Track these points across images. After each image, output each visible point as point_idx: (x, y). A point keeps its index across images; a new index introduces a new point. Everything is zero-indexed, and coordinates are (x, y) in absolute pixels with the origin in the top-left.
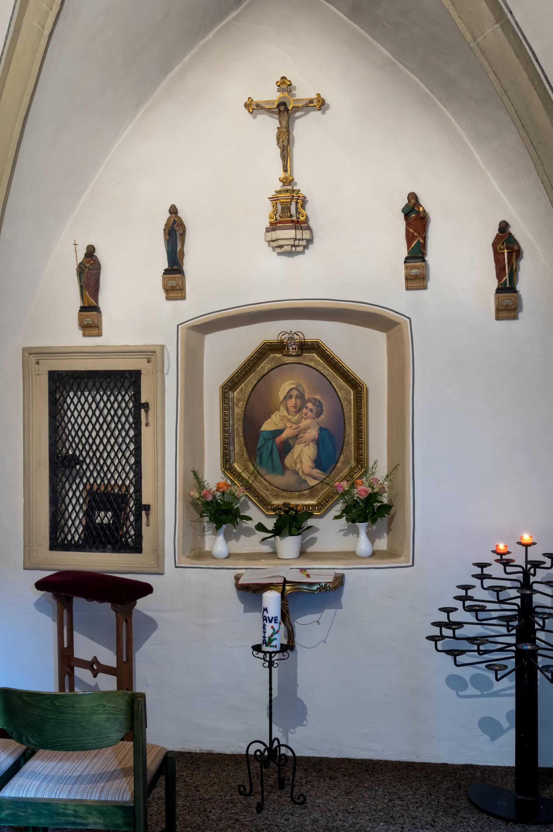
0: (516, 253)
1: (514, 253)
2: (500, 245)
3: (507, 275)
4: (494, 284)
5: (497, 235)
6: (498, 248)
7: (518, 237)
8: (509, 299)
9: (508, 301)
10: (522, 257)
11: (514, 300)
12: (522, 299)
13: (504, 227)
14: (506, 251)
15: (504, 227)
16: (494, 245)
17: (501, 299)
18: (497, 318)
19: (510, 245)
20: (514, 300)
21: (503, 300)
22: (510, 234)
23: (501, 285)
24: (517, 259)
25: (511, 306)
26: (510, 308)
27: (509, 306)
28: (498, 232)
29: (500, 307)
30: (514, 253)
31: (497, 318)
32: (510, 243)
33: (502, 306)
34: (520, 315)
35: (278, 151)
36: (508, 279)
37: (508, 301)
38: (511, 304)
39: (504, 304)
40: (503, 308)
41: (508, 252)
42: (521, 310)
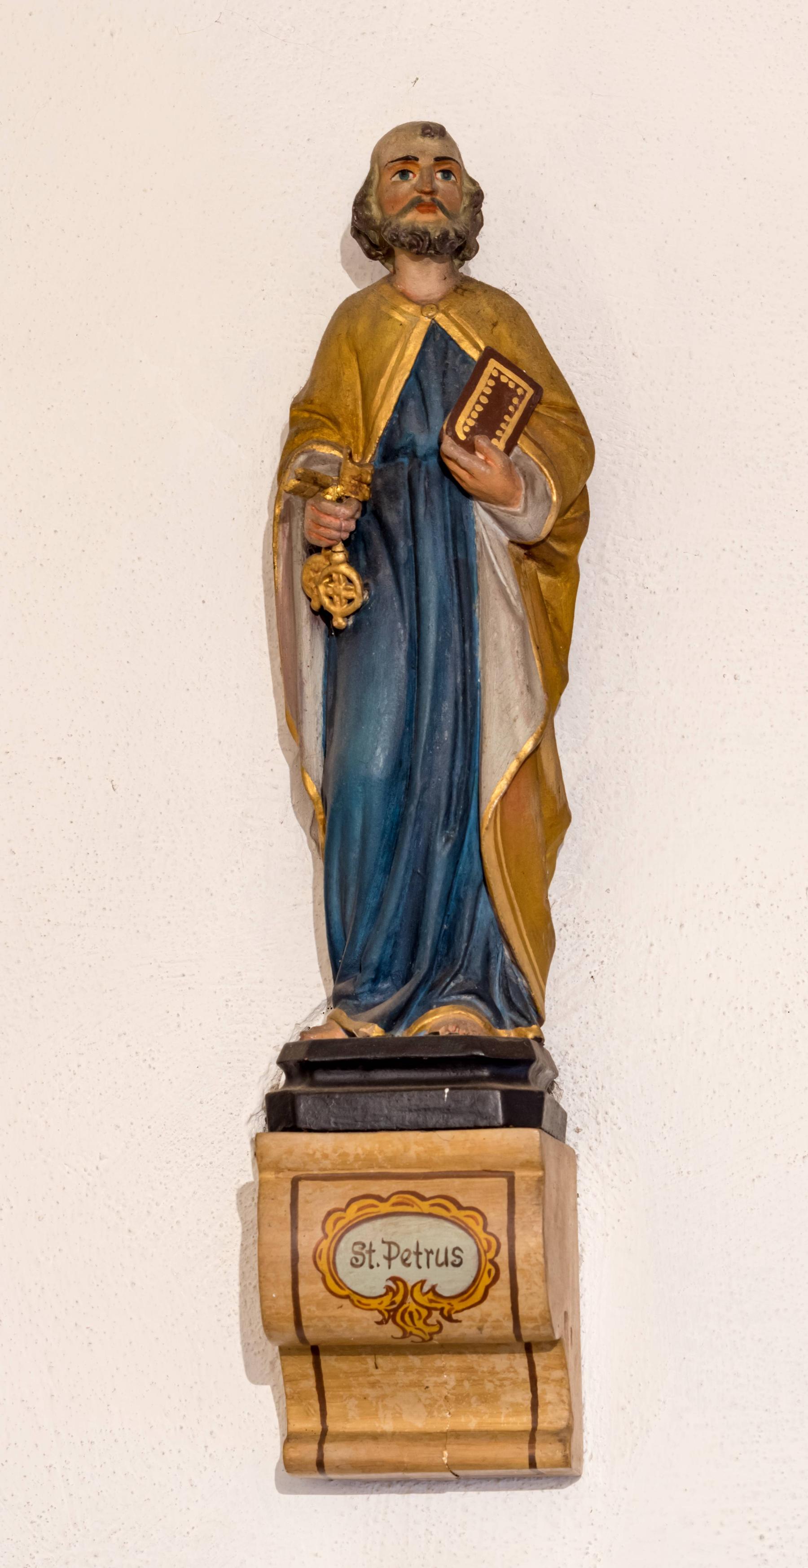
8: (448, 1208)
13: (417, 211)
15: (417, 211)
38: (451, 1281)
39: (371, 1281)
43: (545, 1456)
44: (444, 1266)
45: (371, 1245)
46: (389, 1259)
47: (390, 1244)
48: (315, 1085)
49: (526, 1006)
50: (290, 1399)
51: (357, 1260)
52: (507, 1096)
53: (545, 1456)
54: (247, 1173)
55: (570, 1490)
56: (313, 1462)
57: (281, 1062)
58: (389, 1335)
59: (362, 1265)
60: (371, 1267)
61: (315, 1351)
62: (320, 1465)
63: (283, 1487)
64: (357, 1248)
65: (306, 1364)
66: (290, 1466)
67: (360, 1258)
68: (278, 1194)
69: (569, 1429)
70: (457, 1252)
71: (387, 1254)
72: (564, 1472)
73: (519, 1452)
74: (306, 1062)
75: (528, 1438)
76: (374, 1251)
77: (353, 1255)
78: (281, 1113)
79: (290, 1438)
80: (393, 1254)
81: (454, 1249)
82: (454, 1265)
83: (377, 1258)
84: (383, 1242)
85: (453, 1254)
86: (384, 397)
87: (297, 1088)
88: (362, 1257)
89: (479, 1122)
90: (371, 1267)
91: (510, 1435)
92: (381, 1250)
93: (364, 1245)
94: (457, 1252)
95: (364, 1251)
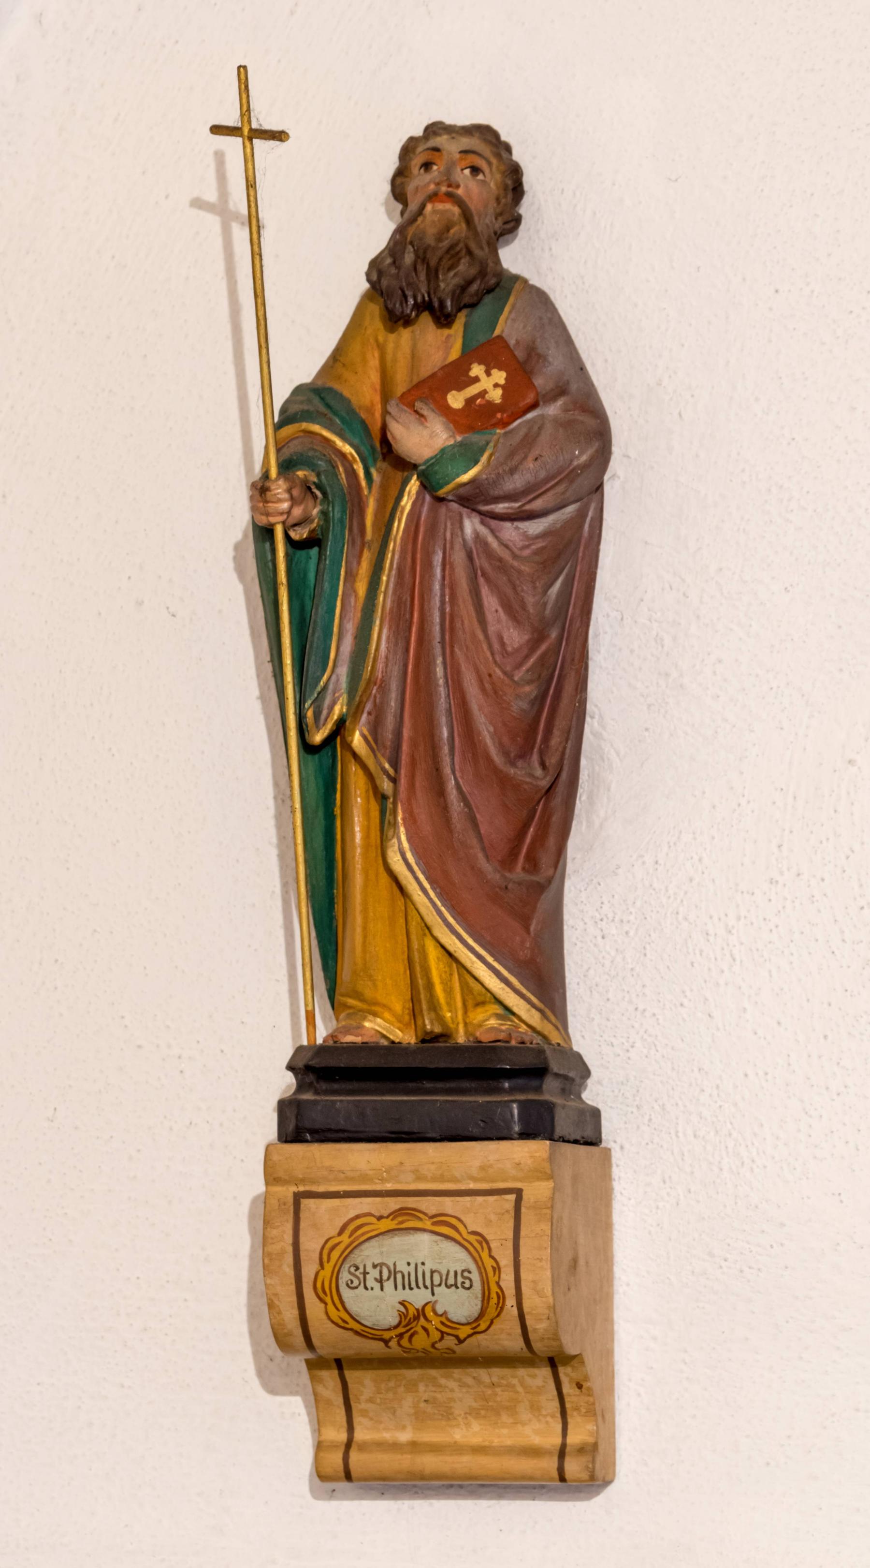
4: (251, 1012)
8: (443, 1226)
13: (454, 246)
15: (454, 246)
43: (576, 1471)
44: (453, 1288)
45: (365, 1267)
46: (380, 1281)
48: (342, 1093)
50: (318, 1408)
51: (352, 1282)
52: (524, 1106)
53: (576, 1471)
54: (256, 1184)
55: (600, 1500)
56: (341, 1471)
57: (290, 1067)
59: (356, 1288)
61: (339, 1364)
62: (348, 1477)
63: (316, 1494)
64: (353, 1269)
65: (330, 1377)
66: (321, 1475)
67: (356, 1282)
68: (286, 1206)
69: (595, 1446)
70: (466, 1274)
72: (595, 1481)
73: (550, 1465)
74: (317, 1069)
78: (298, 1124)
79: (320, 1447)
80: (385, 1276)
81: (463, 1271)
85: (462, 1275)
87: (308, 1096)
89: (496, 1132)
90: (366, 1288)
91: (534, 1452)
94: (466, 1274)
95: (357, 1273)
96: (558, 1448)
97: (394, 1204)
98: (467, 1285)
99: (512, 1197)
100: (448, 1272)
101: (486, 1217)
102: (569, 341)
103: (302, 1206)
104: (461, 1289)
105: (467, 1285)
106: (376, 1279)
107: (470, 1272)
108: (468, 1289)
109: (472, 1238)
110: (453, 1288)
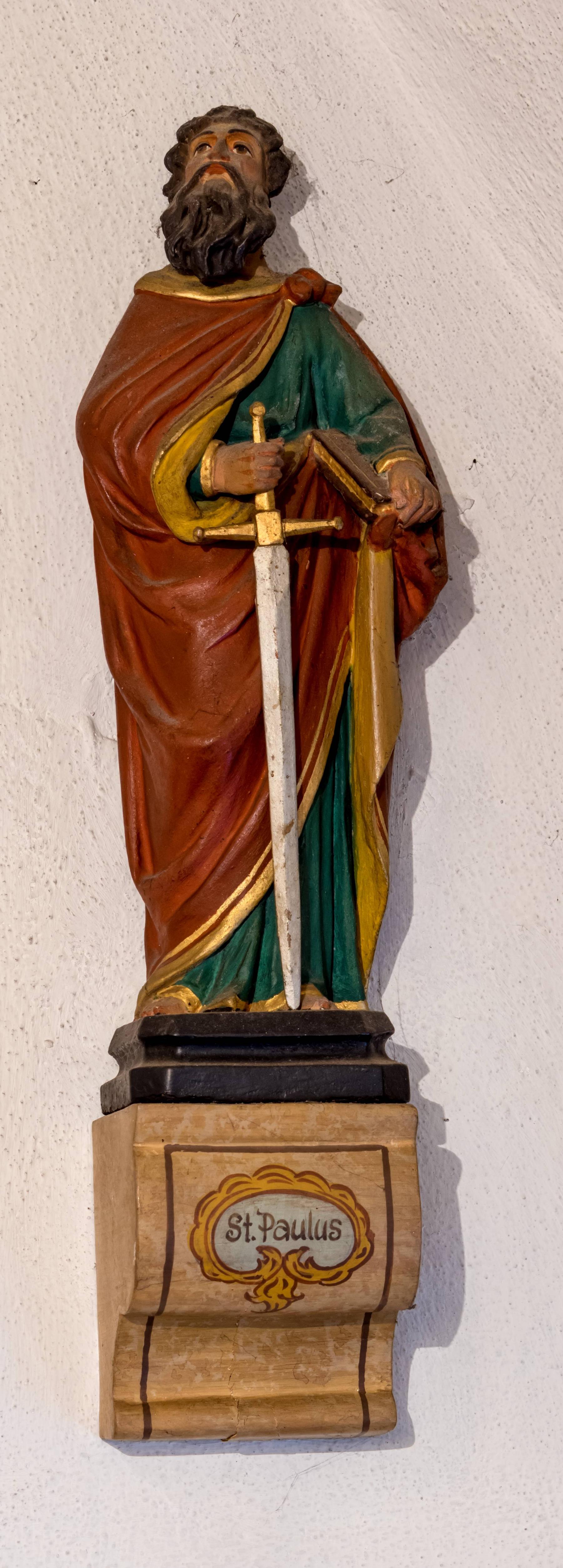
0: (383, 551)
1: (375, 566)
2: (188, 437)
3: (283, 851)
4: (103, 966)
5: (148, 308)
6: (166, 476)
7: (394, 330)
8: (304, 1185)
9: (284, 1209)
10: (471, 611)
11: (371, 1200)
12: (452, 1167)
13: (228, 200)
14: (268, 527)
15: (228, 200)
16: (112, 434)
17: (201, 1174)
18: (135, 1422)
19: (310, 446)
20: (371, 1200)
21: (235, 1188)
22: (317, 297)
23: (200, 977)
24: (401, 630)
25: (336, 1276)
26: (316, 1298)
27: (306, 1270)
28: (158, 259)
29: (192, 1289)
30: (375, 566)
31: (135, 1422)
32: (309, 418)
33: (217, 1269)
34: (430, 1377)
35: (289, 144)
36: (287, 899)
37: (284, 1209)
38: (327, 1253)
39: (242, 1254)
40: (225, 1295)
41: (291, 542)
42: (443, 1328)
44: (322, 1239)
47: (265, 1215)
49: (224, 377)
51: (232, 1233)
58: (249, 1311)
60: (248, 1240)
64: (234, 1220)
67: (236, 1232)
70: (336, 1225)
71: (262, 1226)
75: (146, 1321)
76: (251, 1224)
77: (229, 1229)
80: (269, 1225)
82: (332, 1239)
83: (255, 1231)
84: (259, 1213)
86: (340, 836)
88: (239, 1228)
92: (256, 1221)
93: (240, 1218)
96: (152, 1411)
97: (260, 1160)
98: (335, 1235)
99: (173, 1154)
100: (294, 1224)
101: (361, 1176)
102: (375, 361)
103: (173, 1158)
104: (315, 1240)
105: (335, 1235)
106: (260, 1227)
107: (340, 1223)
108: (338, 1238)
109: (336, 1193)
110: (322, 1239)
